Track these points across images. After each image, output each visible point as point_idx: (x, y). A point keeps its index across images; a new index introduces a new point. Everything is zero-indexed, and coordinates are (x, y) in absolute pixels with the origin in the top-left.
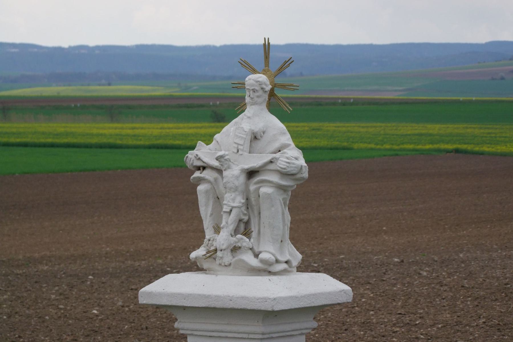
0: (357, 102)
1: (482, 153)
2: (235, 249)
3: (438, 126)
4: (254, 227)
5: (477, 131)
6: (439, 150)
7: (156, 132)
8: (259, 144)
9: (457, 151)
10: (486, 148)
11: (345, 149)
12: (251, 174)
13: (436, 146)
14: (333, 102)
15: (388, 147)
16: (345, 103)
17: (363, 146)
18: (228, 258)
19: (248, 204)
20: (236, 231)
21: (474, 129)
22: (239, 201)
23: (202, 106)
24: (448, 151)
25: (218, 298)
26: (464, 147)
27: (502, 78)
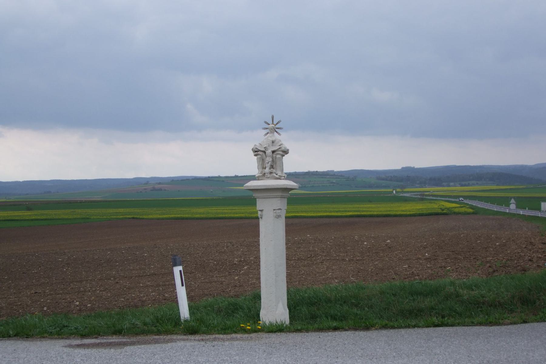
0: (86, 202)
1: (143, 219)
2: (271, 173)
3: (123, 209)
4: (274, 166)
5: (138, 211)
6: (126, 218)
7: (6, 215)
8: (274, 144)
9: (133, 218)
10: (145, 217)
11: (88, 218)
12: (273, 152)
13: (125, 216)
14: (76, 202)
15: (105, 217)
16: (81, 202)
17: (95, 217)
18: (269, 176)
19: (273, 161)
20: (270, 169)
21: (137, 210)
22: (271, 160)
23: (20, 205)
24: (129, 218)
25: (269, 185)
26: (135, 216)
27: (141, 192)
